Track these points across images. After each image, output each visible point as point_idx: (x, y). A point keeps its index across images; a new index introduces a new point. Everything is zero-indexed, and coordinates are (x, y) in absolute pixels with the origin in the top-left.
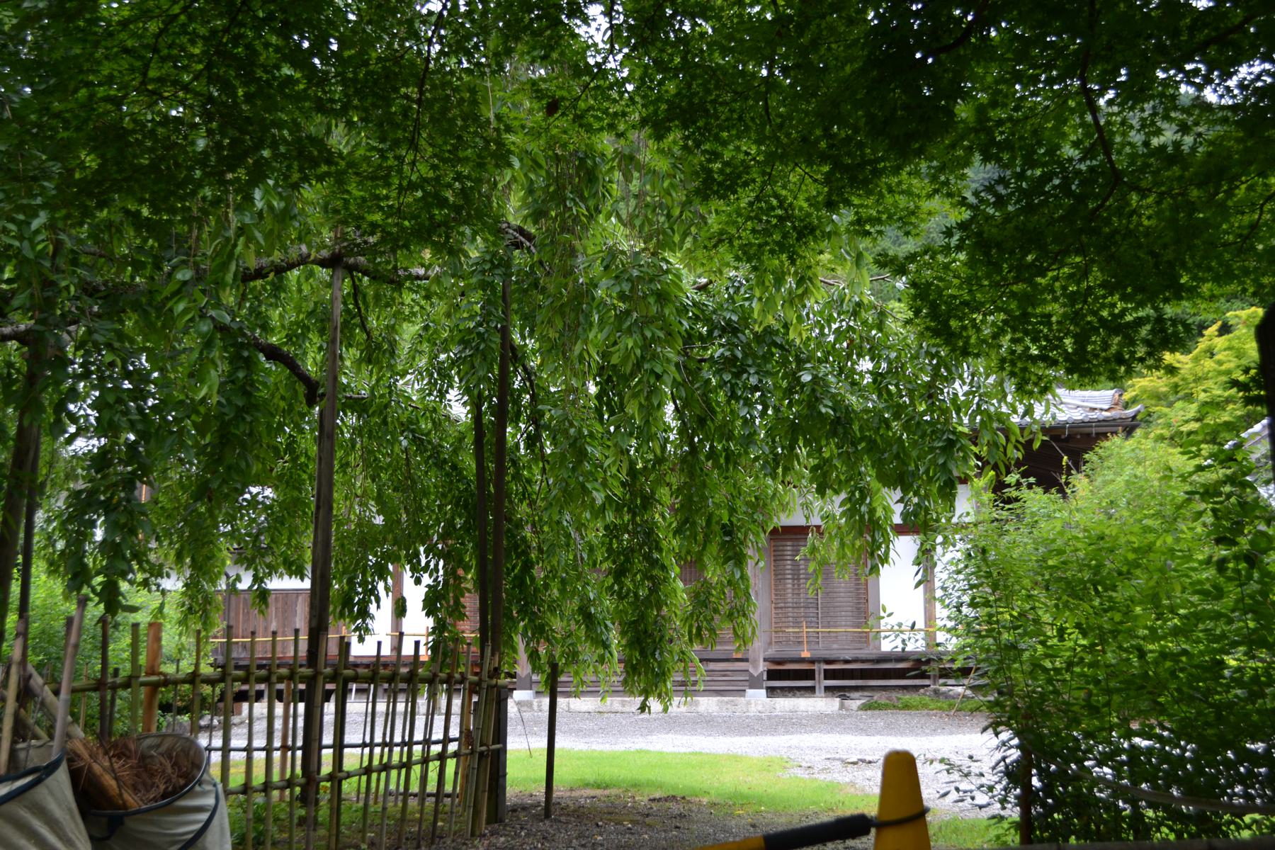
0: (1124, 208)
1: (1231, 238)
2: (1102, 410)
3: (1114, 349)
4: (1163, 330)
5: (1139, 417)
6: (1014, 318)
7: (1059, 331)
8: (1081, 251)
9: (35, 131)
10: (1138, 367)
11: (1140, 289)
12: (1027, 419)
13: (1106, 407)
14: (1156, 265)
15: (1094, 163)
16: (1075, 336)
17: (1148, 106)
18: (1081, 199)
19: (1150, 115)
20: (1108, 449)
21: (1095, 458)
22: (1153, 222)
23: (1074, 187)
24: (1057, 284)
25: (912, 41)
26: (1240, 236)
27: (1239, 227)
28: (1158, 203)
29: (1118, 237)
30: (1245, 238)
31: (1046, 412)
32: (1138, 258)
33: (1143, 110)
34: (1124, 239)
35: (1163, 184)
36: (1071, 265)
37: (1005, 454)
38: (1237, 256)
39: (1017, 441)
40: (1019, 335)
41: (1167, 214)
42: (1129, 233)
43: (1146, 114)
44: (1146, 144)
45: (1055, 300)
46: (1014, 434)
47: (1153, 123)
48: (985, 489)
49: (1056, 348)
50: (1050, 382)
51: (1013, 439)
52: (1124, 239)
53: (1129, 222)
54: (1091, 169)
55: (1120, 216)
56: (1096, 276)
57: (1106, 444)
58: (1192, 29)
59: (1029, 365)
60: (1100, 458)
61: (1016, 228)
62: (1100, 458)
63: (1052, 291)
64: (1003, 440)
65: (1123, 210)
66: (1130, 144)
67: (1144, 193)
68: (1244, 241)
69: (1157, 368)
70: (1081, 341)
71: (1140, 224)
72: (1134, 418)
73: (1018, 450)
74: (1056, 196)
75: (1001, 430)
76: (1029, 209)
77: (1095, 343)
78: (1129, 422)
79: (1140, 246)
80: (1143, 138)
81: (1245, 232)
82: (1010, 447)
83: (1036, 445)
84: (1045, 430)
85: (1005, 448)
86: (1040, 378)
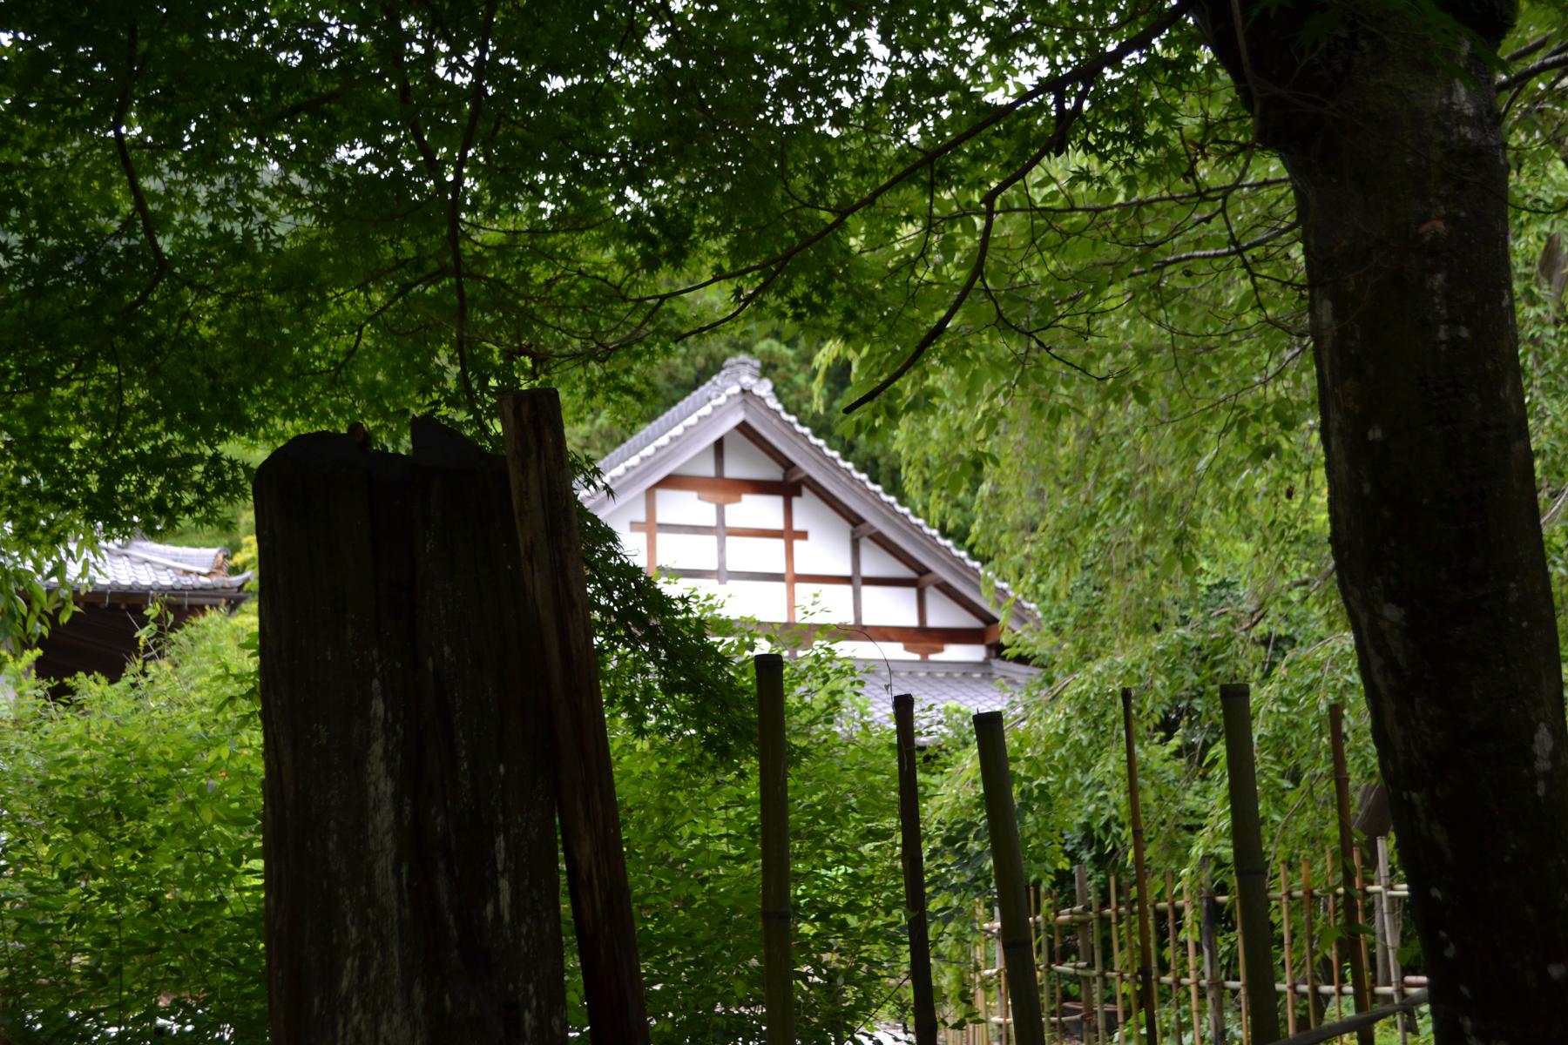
0: (175, 308)
1: (324, 365)
2: (199, 574)
3: (153, 493)
4: (220, 473)
5: (246, 587)
6: (21, 440)
7: (80, 462)
8: (113, 358)
9: (96, 184)
10: (186, 521)
11: (192, 417)
12: (54, 579)
13: (206, 571)
14: (213, 388)
15: (133, 242)
16: (102, 472)
17: (220, 182)
18: (114, 288)
19: (222, 190)
20: (203, 627)
21: (184, 640)
22: (212, 332)
23: (103, 271)
24: (85, 400)
25: (728, 187)
26: (335, 363)
27: (334, 352)
28: (223, 306)
29: (165, 346)
30: (339, 367)
31: (82, 575)
32: (191, 376)
33: (212, 183)
34: (172, 348)
35: (229, 282)
36: (103, 377)
37: (25, 628)
38: (330, 388)
39: (43, 611)
40: (27, 465)
41: (234, 321)
42: (180, 342)
43: (215, 190)
44: (213, 227)
45: (80, 420)
46: (39, 601)
47: (224, 202)
48: (27, 674)
49: (75, 484)
50: (66, 531)
51: (37, 608)
52: (172, 348)
53: (181, 326)
54: (128, 250)
55: (171, 318)
56: (135, 395)
57: (201, 620)
58: (276, 89)
59: (37, 505)
60: (191, 639)
61: (20, 315)
62: (191, 639)
63: (77, 408)
64: (23, 608)
65: (172, 308)
66: (192, 224)
67: (204, 291)
68: (338, 370)
69: (208, 522)
70: (110, 477)
71: (194, 331)
72: (240, 588)
73: (43, 623)
74: (78, 280)
75: (22, 594)
76: (37, 293)
77: (128, 483)
78: (234, 592)
79: (193, 361)
80: (210, 219)
81: (341, 359)
82: (32, 619)
83: (65, 618)
84: (77, 597)
85: (25, 620)
86: (51, 524)
